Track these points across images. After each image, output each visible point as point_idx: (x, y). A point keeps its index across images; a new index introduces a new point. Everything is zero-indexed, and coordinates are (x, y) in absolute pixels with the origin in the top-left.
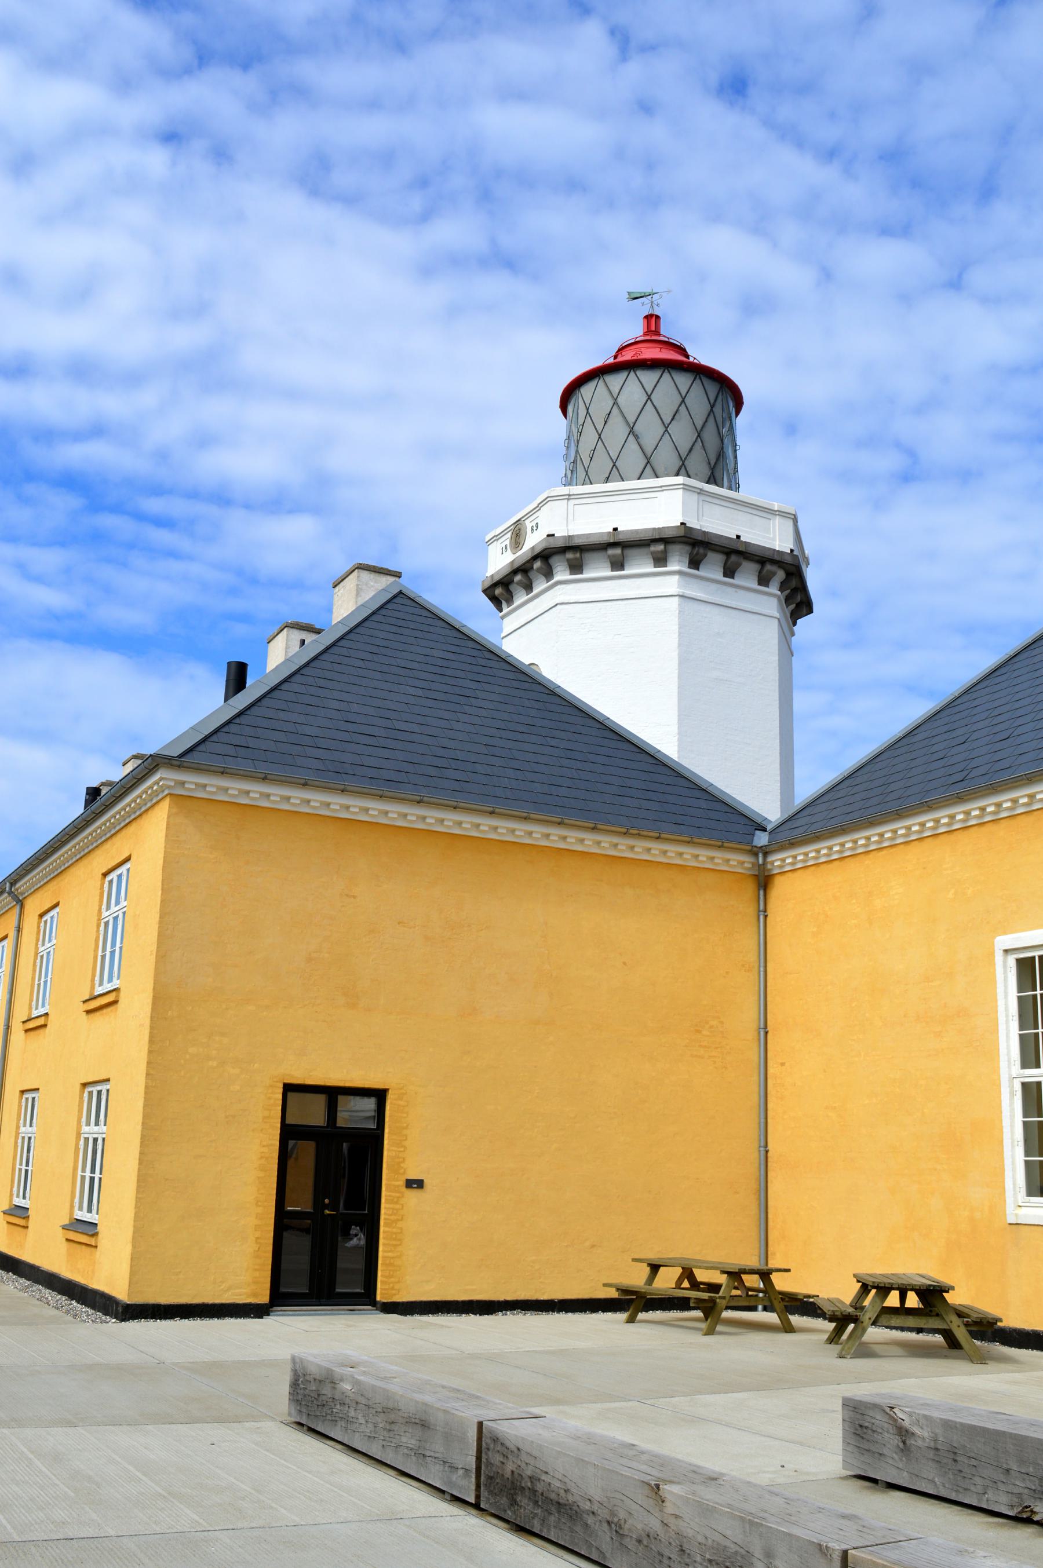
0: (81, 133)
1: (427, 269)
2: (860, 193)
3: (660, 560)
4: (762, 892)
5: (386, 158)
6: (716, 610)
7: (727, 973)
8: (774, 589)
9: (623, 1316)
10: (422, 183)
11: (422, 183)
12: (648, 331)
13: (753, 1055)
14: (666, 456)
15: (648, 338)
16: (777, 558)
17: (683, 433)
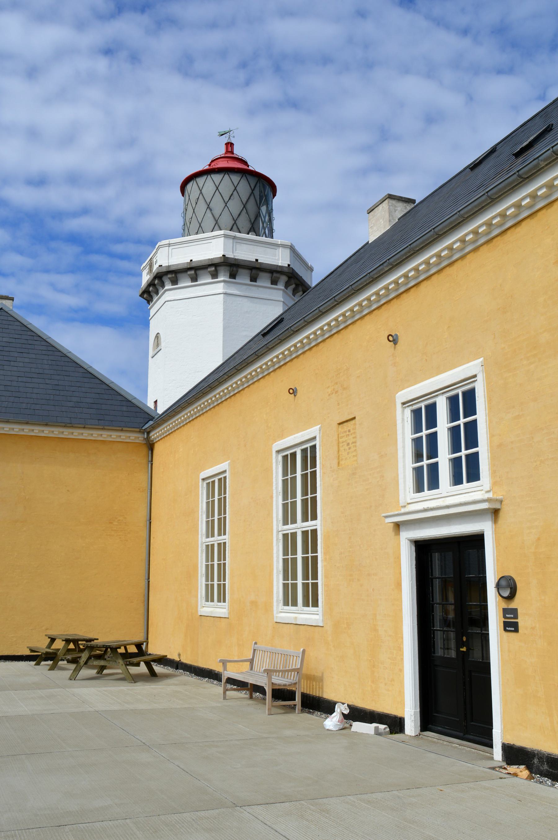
0: (61, 54)
1: (252, 112)
2: (485, 52)
3: (215, 275)
4: (150, 452)
5: (223, 54)
6: (245, 300)
7: (129, 493)
8: (281, 286)
9: (33, 663)
10: (243, 65)
11: (243, 65)
12: (227, 152)
13: (144, 534)
14: (226, 219)
15: (226, 155)
16: (279, 269)
17: (235, 206)
